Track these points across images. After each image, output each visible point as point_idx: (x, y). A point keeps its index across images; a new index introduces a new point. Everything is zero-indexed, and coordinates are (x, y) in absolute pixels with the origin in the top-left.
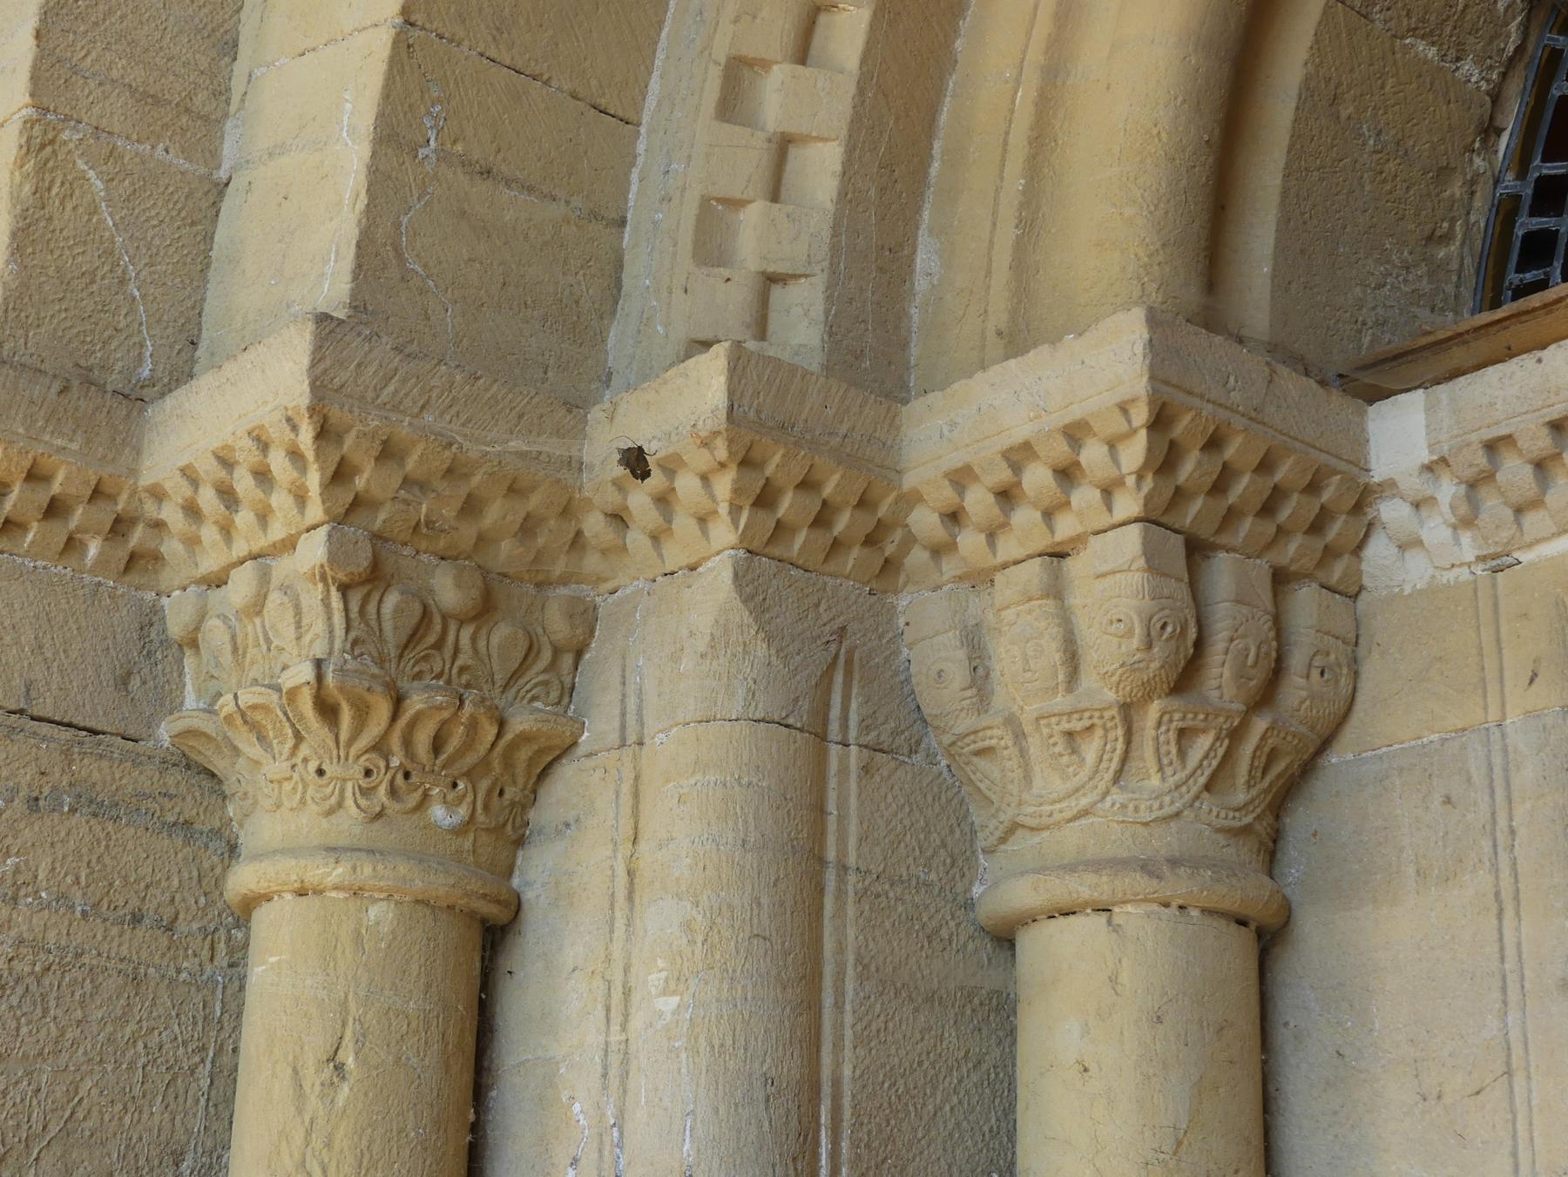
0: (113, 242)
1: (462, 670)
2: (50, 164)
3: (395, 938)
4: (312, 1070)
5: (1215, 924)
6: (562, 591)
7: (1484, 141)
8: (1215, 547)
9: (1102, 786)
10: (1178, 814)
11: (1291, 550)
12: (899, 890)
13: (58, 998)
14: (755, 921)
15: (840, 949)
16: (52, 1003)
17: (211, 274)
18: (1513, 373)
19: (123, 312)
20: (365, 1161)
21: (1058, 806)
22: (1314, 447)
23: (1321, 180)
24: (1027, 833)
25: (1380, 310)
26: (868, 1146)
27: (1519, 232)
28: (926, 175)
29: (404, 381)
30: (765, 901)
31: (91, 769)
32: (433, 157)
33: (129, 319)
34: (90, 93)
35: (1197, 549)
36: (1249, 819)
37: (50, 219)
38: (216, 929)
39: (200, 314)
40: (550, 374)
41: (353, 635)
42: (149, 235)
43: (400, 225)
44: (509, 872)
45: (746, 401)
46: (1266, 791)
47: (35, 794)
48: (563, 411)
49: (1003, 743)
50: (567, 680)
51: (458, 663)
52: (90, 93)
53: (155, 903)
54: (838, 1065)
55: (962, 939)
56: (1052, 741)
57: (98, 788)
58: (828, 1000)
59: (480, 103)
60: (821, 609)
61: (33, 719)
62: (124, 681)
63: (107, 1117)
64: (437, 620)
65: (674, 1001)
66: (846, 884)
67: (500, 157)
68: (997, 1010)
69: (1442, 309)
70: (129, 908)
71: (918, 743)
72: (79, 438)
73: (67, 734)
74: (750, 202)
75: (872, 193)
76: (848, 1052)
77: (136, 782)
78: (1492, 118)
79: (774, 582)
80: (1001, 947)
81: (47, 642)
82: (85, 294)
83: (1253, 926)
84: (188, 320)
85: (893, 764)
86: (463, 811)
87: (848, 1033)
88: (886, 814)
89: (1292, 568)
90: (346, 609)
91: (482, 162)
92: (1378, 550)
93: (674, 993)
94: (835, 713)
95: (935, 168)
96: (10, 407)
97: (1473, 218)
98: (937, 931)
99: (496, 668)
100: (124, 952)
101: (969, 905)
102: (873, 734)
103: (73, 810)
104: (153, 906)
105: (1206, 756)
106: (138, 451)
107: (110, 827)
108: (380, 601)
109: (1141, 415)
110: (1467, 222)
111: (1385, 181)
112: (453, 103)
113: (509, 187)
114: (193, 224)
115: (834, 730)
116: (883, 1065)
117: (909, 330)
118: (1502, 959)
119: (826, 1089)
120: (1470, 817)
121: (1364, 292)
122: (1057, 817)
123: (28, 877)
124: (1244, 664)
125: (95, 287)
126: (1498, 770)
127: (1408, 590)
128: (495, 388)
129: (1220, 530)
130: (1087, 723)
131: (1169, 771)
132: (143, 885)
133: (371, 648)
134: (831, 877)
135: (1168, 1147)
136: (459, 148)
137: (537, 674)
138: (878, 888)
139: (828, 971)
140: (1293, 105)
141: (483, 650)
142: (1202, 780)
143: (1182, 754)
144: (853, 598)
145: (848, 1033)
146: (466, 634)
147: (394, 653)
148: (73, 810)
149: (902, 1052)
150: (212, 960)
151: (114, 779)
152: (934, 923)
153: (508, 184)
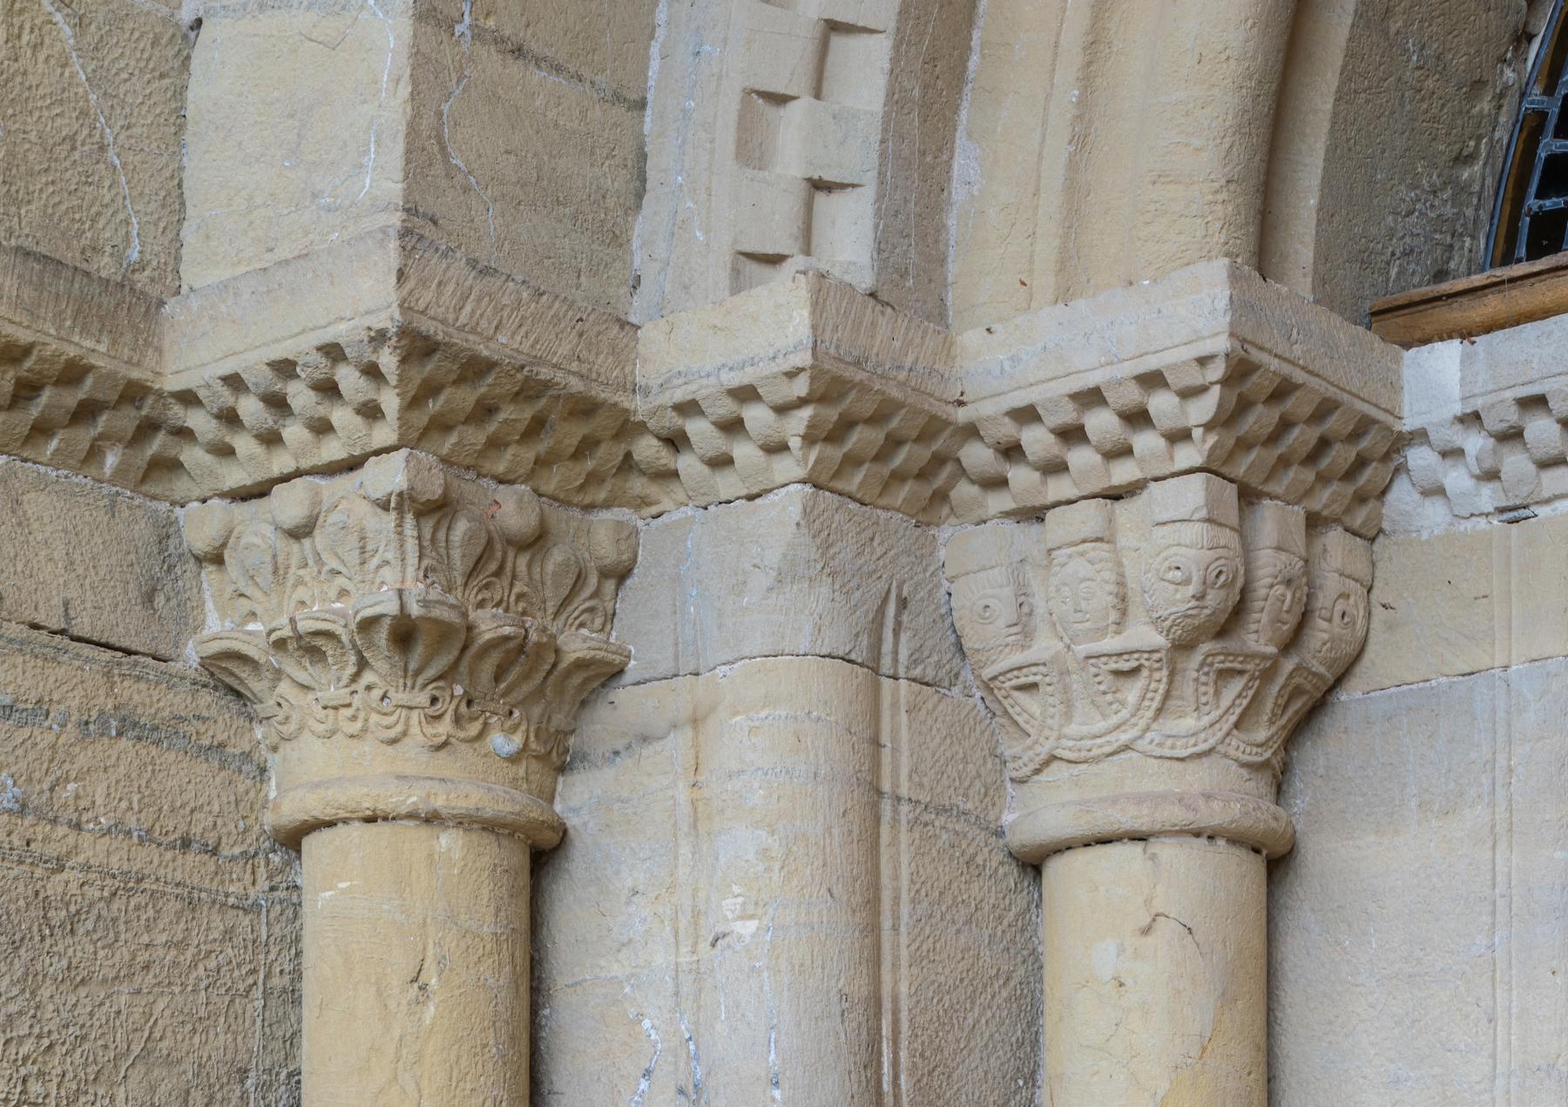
0: (87, 101)
1: (520, 596)
4: (396, 991)
5: (1237, 852)
6: (605, 515)
7: (1516, 49)
8: (1260, 495)
9: (1142, 723)
13: (126, 922)
16: (122, 928)
17: (188, 137)
18: (1551, 333)
19: (107, 184)
20: (455, 1074)
21: (1098, 741)
22: (1358, 397)
23: (1367, 102)
24: (1064, 764)
25: (1408, 239)
26: (922, 1055)
27: (1542, 154)
28: (965, 68)
29: (479, 300)
31: (132, 693)
32: (468, 33)
33: (113, 192)
35: (1248, 496)
36: (1268, 754)
37: (25, 73)
38: (256, 853)
39: (180, 186)
40: (583, 278)
41: (426, 562)
42: (122, 90)
44: (551, 800)
45: (827, 337)
46: (1284, 727)
47: (85, 718)
48: (616, 329)
49: (1047, 679)
50: (609, 606)
51: (516, 590)
54: (896, 982)
55: (994, 864)
56: (1099, 679)
58: (886, 923)
60: (875, 544)
61: (73, 639)
62: (149, 597)
63: (179, 1037)
64: (498, 546)
65: (752, 925)
67: (530, 32)
68: (1022, 931)
69: (1461, 235)
71: (957, 675)
72: (105, 339)
73: (109, 654)
74: (793, 98)
75: (916, 92)
76: (904, 971)
78: (1526, 24)
79: (837, 517)
80: (1025, 871)
81: (77, 557)
82: (68, 163)
83: (1265, 852)
84: (169, 194)
86: (518, 740)
87: (904, 953)
89: (1325, 513)
90: (419, 538)
92: (1402, 495)
93: (752, 917)
94: (887, 646)
95: (974, 61)
96: (39, 305)
97: (1497, 135)
99: (548, 593)
100: (179, 877)
101: (999, 833)
102: (920, 668)
103: (120, 734)
104: (199, 830)
105: (1239, 696)
106: (159, 350)
107: (154, 751)
108: (449, 528)
109: (1217, 371)
110: (1491, 139)
111: (1423, 100)
113: (539, 67)
114: (162, 76)
115: (886, 664)
116: (933, 983)
117: (947, 245)
118: (1494, 886)
119: (887, 1005)
120: (1473, 755)
121: (1395, 221)
122: (1095, 752)
125: (77, 155)
126: (1501, 714)
127: (1425, 536)
128: (557, 305)
129: (1267, 480)
130: (1134, 664)
134: (886, 807)
135: (1195, 1051)
136: (491, 23)
138: (926, 817)
139: (886, 897)
140: (1349, 21)
141: (537, 577)
142: (1233, 719)
145: (904, 953)
146: (522, 561)
147: (460, 581)
148: (120, 734)
149: (947, 971)
150: (254, 883)
152: (971, 850)
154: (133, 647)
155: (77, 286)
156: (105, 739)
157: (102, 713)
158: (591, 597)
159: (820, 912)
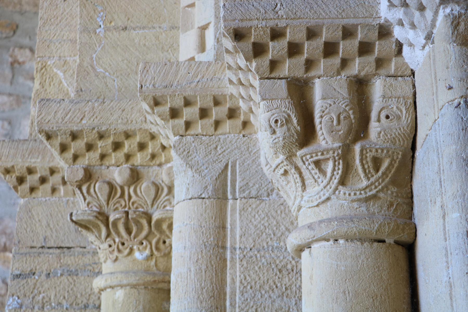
2: (45, 74)
3: (124, 302)
10: (328, 199)
11: (356, 67)
12: (262, 253)
14: (189, 277)
15: (233, 281)
29: (74, 113)
30: (192, 269)
32: (103, 31)
34: (57, 47)
37: (46, 90)
43: (92, 58)
47: (48, 272)
51: (132, 201)
52: (57, 47)
53: (92, 300)
57: (70, 266)
59: (118, 6)
66: (235, 255)
70: (83, 303)
77: (84, 261)
79: (193, 145)
85: (258, 202)
86: (147, 252)
88: (255, 223)
89: (363, 74)
91: (123, 26)
98: (285, 266)
103: (62, 275)
107: (75, 278)
112: (107, 10)
113: (135, 30)
123: (47, 299)
124: (332, 126)
128: (112, 104)
131: (320, 181)
132: (88, 295)
133: (95, 203)
136: (113, 24)
137: (164, 197)
143: (323, 172)
144: (234, 140)
147: (105, 203)
148: (62, 275)
151: (76, 262)
153: (134, 29)
154: (70, 246)
155: (31, 145)
156: (56, 278)
157: (55, 269)
158: (167, 195)
159: (185, 304)
